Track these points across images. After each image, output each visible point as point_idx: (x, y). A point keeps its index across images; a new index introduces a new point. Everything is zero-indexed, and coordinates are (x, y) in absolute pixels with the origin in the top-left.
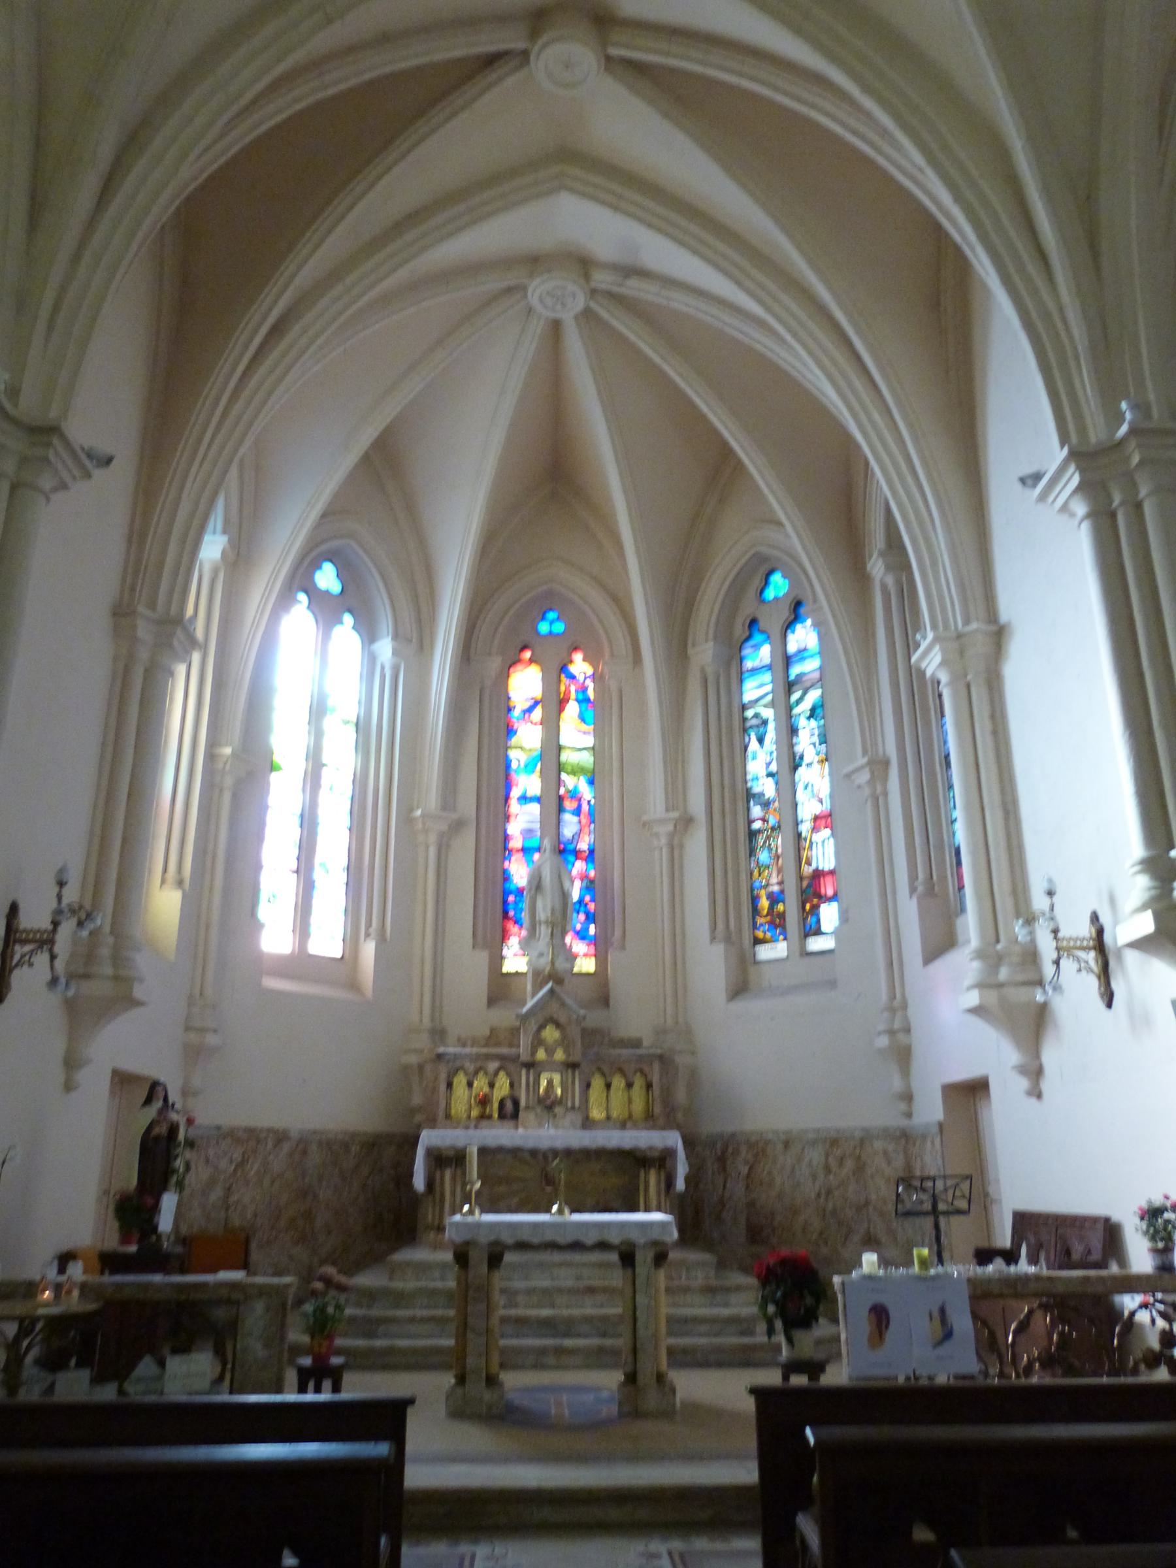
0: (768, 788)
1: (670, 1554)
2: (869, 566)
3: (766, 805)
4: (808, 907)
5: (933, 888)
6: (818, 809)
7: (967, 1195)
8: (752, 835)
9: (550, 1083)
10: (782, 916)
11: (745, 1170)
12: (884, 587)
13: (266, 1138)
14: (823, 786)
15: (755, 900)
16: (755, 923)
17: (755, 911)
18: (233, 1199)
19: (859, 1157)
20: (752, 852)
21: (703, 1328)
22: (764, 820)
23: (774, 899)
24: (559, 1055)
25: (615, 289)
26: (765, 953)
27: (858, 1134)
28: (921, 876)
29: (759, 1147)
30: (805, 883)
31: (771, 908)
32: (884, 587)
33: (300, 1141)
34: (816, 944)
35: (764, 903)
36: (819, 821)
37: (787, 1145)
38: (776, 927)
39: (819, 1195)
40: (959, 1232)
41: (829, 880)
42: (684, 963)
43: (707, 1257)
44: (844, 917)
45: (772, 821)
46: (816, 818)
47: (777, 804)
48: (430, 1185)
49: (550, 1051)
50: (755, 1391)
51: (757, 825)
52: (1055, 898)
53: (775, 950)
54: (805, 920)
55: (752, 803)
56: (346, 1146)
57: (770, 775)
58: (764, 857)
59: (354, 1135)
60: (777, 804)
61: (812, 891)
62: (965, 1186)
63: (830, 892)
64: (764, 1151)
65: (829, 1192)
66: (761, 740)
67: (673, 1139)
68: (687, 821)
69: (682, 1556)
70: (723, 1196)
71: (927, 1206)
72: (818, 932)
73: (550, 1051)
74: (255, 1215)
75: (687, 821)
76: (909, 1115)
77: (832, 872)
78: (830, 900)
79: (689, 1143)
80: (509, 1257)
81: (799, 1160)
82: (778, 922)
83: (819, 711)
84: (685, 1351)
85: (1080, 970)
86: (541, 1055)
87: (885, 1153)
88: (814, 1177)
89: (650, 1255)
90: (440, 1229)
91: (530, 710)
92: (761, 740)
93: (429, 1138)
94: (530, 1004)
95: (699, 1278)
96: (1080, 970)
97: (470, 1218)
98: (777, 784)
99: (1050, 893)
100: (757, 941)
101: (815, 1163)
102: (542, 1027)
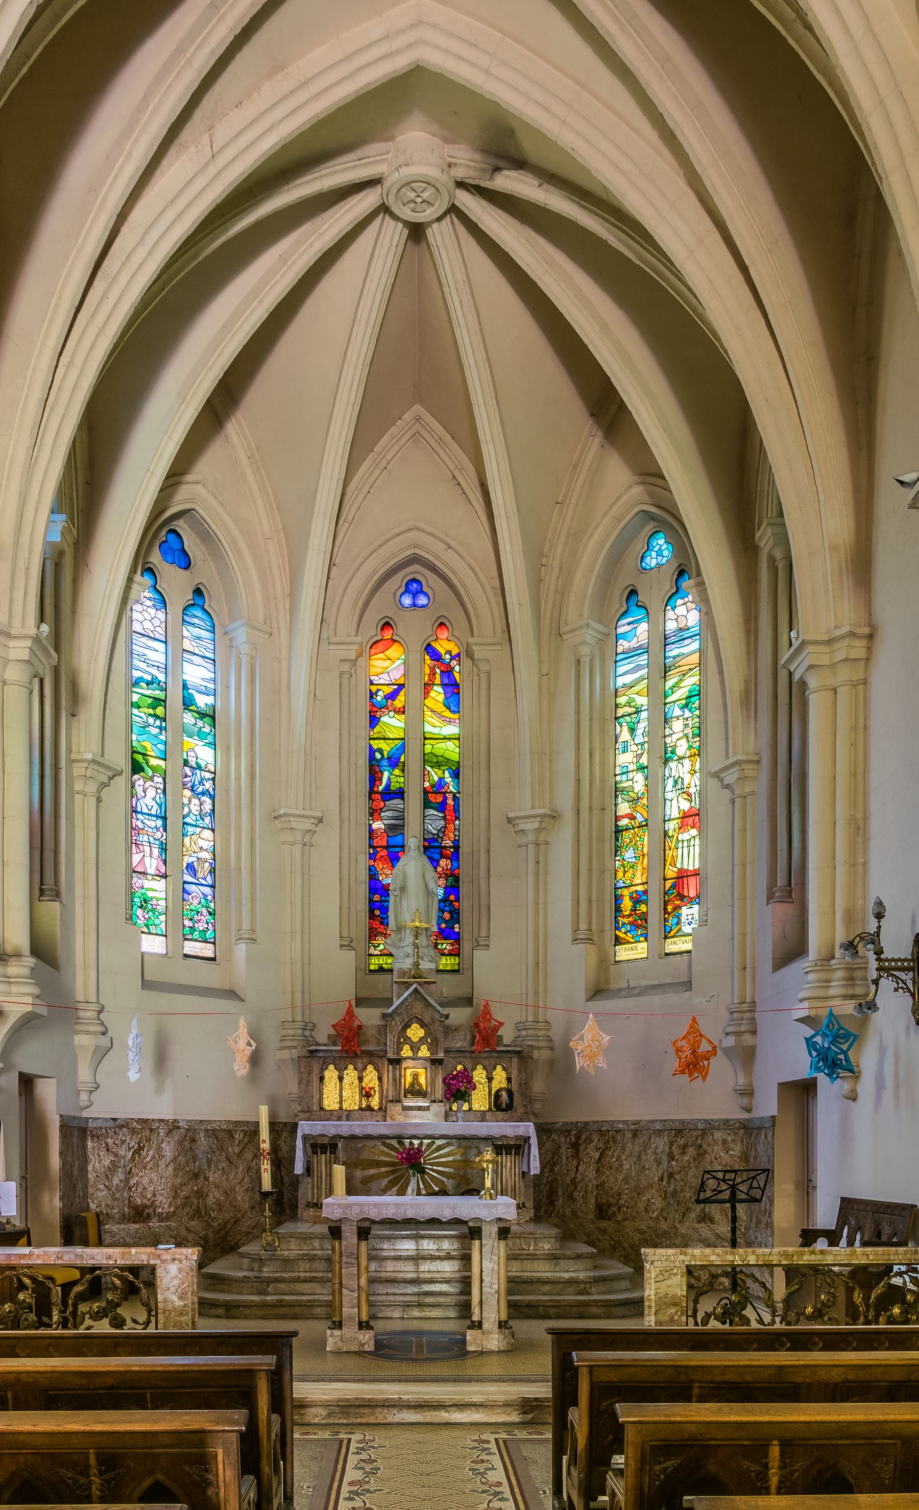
0: (639, 783)
1: (496, 1440)
2: (757, 535)
3: (635, 801)
4: (670, 908)
5: (790, 892)
6: (685, 806)
7: (762, 1186)
8: (618, 831)
9: (416, 1076)
10: (644, 917)
11: (597, 1155)
12: (772, 560)
13: (158, 1128)
14: (693, 783)
15: (618, 899)
16: (617, 922)
17: (618, 909)
18: (133, 1181)
19: (701, 1146)
20: (617, 850)
21: (547, 1288)
22: (632, 817)
23: (636, 900)
24: (424, 1052)
25: (483, 184)
26: (624, 953)
27: (701, 1126)
28: (780, 883)
29: (609, 1135)
30: (669, 884)
31: (634, 910)
32: (772, 560)
33: (188, 1130)
34: (673, 946)
35: (627, 904)
36: (686, 818)
37: (635, 1134)
38: (638, 927)
39: (662, 1179)
40: (783, 1210)
41: (692, 881)
42: (545, 962)
43: (554, 1231)
44: (703, 922)
45: (640, 818)
46: (685, 816)
47: (645, 801)
48: (308, 1170)
49: (415, 1048)
50: (552, 1332)
51: (624, 822)
52: (883, 922)
53: (633, 951)
54: (666, 920)
55: (620, 800)
56: (230, 1133)
57: (642, 768)
58: (629, 855)
59: (237, 1123)
60: (645, 801)
61: (677, 891)
62: (762, 1178)
63: (692, 894)
64: (614, 1140)
65: (671, 1175)
66: (632, 731)
67: (528, 1129)
68: (554, 817)
69: (505, 1442)
70: (575, 1178)
71: (726, 1195)
72: (679, 934)
73: (415, 1048)
74: (154, 1195)
75: (554, 817)
76: (748, 1110)
77: (696, 873)
78: (691, 900)
79: (542, 1130)
80: (376, 1231)
81: (646, 1147)
82: (640, 923)
83: (696, 702)
84: (529, 1305)
85: (896, 990)
86: (406, 1051)
87: (724, 1142)
88: (658, 1162)
89: (495, 1229)
90: (318, 1206)
91: (392, 696)
92: (632, 731)
93: (305, 1127)
94: (396, 1003)
95: (547, 1246)
96: (896, 990)
97: (339, 1203)
98: (646, 778)
99: (879, 916)
100: (618, 941)
101: (659, 1150)
102: (407, 1026)
